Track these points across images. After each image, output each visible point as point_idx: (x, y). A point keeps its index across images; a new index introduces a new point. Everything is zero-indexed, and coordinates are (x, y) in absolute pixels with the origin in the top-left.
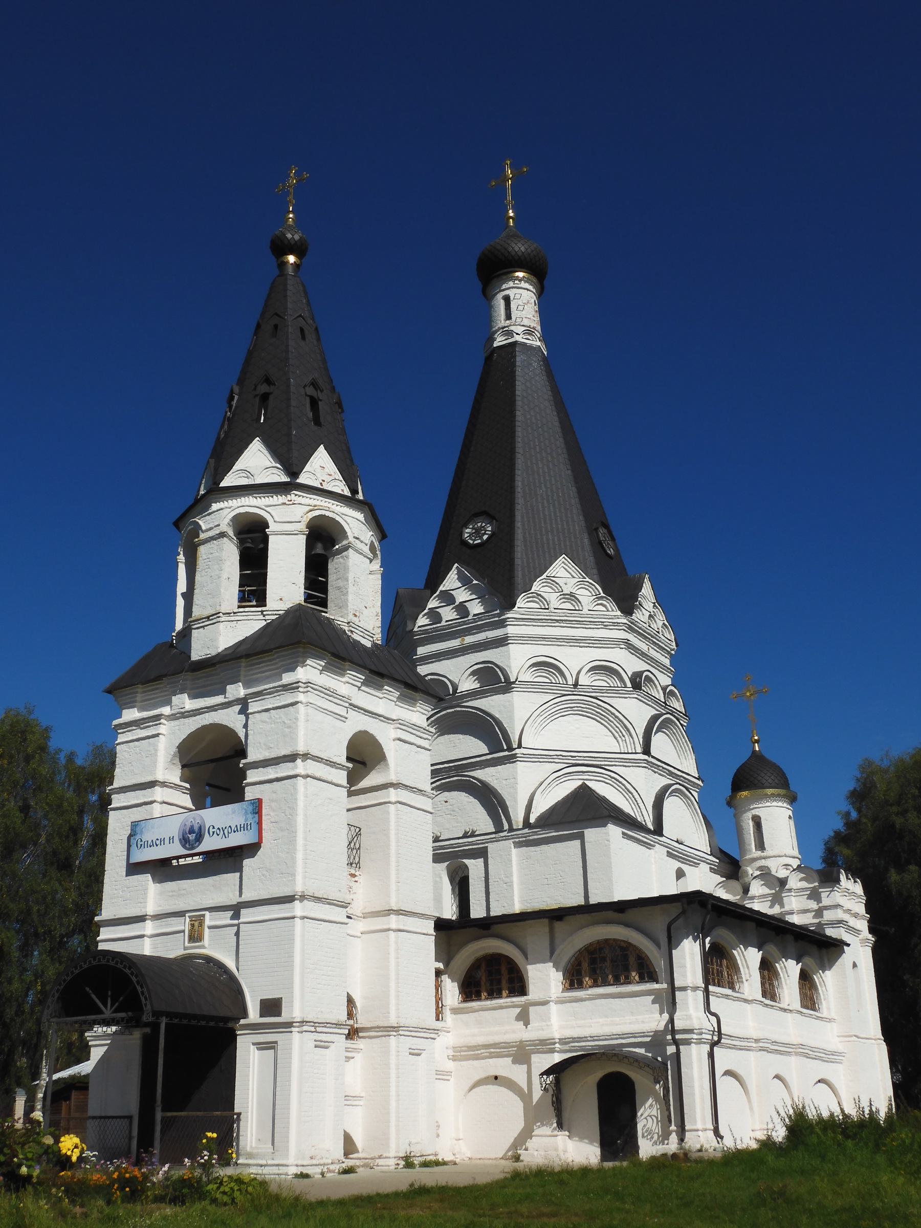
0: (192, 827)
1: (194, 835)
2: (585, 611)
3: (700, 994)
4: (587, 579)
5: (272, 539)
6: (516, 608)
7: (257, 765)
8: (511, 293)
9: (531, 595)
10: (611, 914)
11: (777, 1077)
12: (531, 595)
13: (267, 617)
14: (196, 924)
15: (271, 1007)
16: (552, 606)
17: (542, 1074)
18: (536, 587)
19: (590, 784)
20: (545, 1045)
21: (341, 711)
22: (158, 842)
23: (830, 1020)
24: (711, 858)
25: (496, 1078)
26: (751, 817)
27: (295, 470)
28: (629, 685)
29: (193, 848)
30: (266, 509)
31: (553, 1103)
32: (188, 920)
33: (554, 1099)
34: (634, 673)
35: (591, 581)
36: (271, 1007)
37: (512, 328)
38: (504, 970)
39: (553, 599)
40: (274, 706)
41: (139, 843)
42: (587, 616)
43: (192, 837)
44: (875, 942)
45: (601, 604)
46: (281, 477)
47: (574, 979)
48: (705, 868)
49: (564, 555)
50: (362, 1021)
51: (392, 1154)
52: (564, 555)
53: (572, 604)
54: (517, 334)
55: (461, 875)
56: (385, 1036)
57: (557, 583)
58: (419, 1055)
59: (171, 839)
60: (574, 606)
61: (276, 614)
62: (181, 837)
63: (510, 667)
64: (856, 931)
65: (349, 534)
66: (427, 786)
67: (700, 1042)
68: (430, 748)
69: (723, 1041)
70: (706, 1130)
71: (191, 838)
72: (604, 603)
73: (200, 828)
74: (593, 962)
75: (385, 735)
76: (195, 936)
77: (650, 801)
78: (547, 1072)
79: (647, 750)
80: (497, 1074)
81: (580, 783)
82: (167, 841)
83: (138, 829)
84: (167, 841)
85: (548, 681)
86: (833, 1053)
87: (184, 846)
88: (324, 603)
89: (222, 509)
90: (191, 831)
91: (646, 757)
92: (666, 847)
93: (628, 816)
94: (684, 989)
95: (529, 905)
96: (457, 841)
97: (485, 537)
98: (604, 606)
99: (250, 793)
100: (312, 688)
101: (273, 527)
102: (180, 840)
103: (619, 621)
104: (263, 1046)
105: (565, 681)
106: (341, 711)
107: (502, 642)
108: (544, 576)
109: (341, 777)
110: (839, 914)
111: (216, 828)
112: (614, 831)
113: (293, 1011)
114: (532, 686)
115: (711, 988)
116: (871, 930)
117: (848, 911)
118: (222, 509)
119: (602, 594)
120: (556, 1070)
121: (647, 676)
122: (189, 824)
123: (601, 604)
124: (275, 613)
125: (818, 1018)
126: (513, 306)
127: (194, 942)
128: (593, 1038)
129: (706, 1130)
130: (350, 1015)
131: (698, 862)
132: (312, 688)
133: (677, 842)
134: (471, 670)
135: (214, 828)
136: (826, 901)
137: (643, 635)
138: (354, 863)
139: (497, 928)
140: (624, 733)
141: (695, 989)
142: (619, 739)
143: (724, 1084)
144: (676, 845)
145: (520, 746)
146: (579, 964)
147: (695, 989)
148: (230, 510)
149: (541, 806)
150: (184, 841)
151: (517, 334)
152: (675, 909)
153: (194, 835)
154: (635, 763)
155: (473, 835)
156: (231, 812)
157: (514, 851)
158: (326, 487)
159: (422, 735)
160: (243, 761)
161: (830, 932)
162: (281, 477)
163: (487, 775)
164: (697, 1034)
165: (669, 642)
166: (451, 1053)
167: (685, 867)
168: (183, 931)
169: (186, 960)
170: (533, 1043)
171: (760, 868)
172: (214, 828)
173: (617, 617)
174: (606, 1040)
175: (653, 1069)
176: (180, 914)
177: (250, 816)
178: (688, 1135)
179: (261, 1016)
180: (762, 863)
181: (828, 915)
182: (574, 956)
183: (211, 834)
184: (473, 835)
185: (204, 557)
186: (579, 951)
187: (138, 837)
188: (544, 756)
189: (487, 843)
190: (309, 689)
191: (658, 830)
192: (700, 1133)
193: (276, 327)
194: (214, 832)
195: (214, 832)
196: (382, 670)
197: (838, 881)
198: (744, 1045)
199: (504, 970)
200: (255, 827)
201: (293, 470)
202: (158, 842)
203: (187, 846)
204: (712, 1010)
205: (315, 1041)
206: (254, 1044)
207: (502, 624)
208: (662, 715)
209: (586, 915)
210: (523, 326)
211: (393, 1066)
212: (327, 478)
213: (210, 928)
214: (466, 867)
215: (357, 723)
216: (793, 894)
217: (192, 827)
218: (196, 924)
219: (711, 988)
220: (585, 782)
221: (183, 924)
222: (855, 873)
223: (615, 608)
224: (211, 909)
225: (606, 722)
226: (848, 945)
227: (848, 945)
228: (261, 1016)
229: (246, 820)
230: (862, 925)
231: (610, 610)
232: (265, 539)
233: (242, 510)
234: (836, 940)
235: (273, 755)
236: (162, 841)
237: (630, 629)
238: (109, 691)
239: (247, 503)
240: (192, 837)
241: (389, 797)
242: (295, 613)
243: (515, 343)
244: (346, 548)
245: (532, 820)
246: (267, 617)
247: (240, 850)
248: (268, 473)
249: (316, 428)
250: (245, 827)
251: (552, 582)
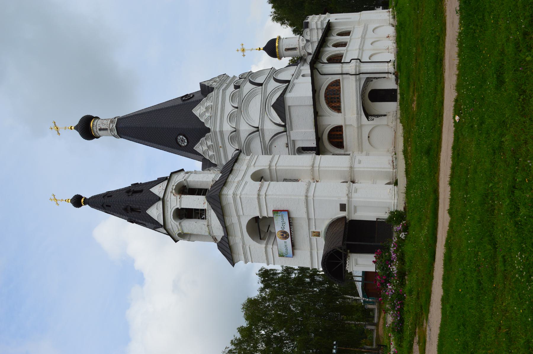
0: (281, 235)
1: (284, 234)
2: (212, 104)
3: (345, 65)
4: (201, 103)
5: (183, 207)
6: (210, 128)
7: (261, 212)
8: (98, 128)
9: (206, 122)
10: (316, 95)
11: (372, 44)
12: (206, 122)
13: (210, 209)
14: (314, 234)
15: (343, 207)
16: (210, 115)
17: (368, 120)
18: (203, 120)
19: (272, 104)
20: (359, 119)
21: (244, 183)
22: (286, 247)
23: (354, 28)
24: (299, 66)
25: (369, 137)
26: (285, 52)
27: (158, 198)
28: (238, 90)
29: (288, 235)
30: (172, 208)
31: (377, 117)
32: (312, 237)
33: (376, 117)
34: (235, 88)
35: (202, 102)
36: (343, 207)
37: (111, 128)
38: (334, 133)
39: (207, 114)
40: (241, 206)
41: (286, 254)
42: (214, 103)
43: (285, 235)
44: (329, 13)
45: (210, 98)
46: (160, 203)
47: (338, 109)
48: (302, 68)
49: (192, 111)
50: (349, 179)
51: (392, 170)
52: (194, 148)
53: (209, 108)
54: (113, 126)
55: (301, 150)
56: (354, 172)
57: (202, 113)
58: (360, 161)
59: (285, 242)
60: (210, 108)
61: (209, 206)
62: (284, 239)
63: (231, 130)
64: (325, 19)
65: (181, 180)
66: (271, 156)
67: (359, 67)
68: (257, 155)
69: (360, 58)
70: (388, 66)
71: (285, 235)
72: (209, 97)
73: (282, 232)
74: (332, 102)
75: (252, 170)
76: (318, 234)
77: (278, 84)
78: (368, 118)
79: (260, 85)
80: (367, 136)
81: (272, 108)
82: (286, 244)
83: (281, 254)
84: (286, 244)
85: (238, 98)
86: (365, 27)
87: (288, 238)
88: (206, 190)
89: (171, 224)
90: (283, 235)
91: (264, 85)
92: (295, 79)
93: (283, 91)
94: (342, 70)
95: (312, 126)
96: (290, 151)
97: (185, 138)
98: (210, 97)
99: (271, 215)
100: (235, 192)
101: (178, 206)
102: (286, 239)
103: (216, 92)
104: (355, 211)
105: (238, 92)
106: (244, 183)
107: (221, 132)
108: (199, 118)
109: (266, 184)
110: (319, 23)
111: (282, 226)
112: (288, 95)
113: (344, 201)
114: (237, 123)
115: (342, 61)
116: (325, 13)
117: (318, 20)
118: (171, 224)
119: (207, 98)
120: (367, 115)
121: (236, 84)
122: (280, 236)
123: (210, 98)
124: (208, 206)
125: (353, 32)
126: (103, 127)
127: (320, 235)
128: (357, 102)
129: (388, 66)
130: (347, 182)
131: (300, 70)
132: (235, 192)
133: (293, 76)
134: (231, 144)
135: (282, 227)
136: (315, 27)
137: (221, 85)
138: (297, 180)
139: (320, 135)
140: (255, 92)
141: (342, 67)
142: (257, 94)
143: (374, 59)
144: (294, 76)
145: (258, 128)
146: (333, 106)
147: (342, 67)
148: (172, 222)
149: (279, 120)
150: (286, 238)
151: (113, 126)
152: (316, 72)
153: (284, 234)
154: (266, 88)
155: (293, 75)
156: (277, 221)
157: (294, 131)
158: (164, 188)
159: (253, 158)
160: (260, 217)
161: (325, 26)
162: (160, 203)
163: (267, 138)
164: (357, 67)
165: (224, 77)
166: (360, 152)
167: (302, 74)
168: (316, 238)
169: (326, 239)
170: (358, 124)
171: (303, 49)
172: (282, 227)
173: (215, 93)
174: (358, 98)
175: (368, 81)
176: (310, 239)
177: (278, 214)
178: (390, 71)
179: (345, 211)
180: (301, 49)
181: (319, 26)
182: (330, 109)
183: (284, 228)
184: (293, 75)
185: (188, 231)
186: (328, 107)
187: (284, 254)
188: (262, 119)
189: (291, 140)
190: (235, 193)
191: (288, 82)
192: (389, 68)
193: (107, 206)
194: (283, 227)
195: (283, 227)
196: (230, 169)
197: (308, 22)
198: (361, 49)
199: (334, 133)
200: (282, 213)
201: (158, 199)
202: (286, 247)
203: (288, 237)
204: (349, 61)
205: (354, 193)
206: (354, 214)
207: (215, 132)
208: (249, 79)
209: (316, 103)
210: (110, 124)
211: (364, 169)
212: (161, 188)
213: (315, 229)
214: (298, 148)
215: (248, 178)
216: (312, 38)
217: (281, 235)
218: (314, 234)
219: (342, 61)
220: (271, 105)
221: (314, 239)
222: (306, 17)
223: (211, 93)
224: (309, 229)
225: (251, 98)
226: (329, 20)
227: (329, 20)
228: (345, 211)
229: (280, 216)
230: (323, 16)
231: (212, 95)
232: (182, 209)
233: (172, 217)
234: (327, 24)
235: (258, 206)
236: (286, 246)
237: (218, 88)
238: (233, 265)
239: (169, 216)
240: (285, 235)
241: (274, 169)
242: (209, 200)
243: (116, 127)
244: (187, 181)
245: (283, 124)
246: (210, 209)
247: (290, 219)
248: (159, 208)
249: (144, 191)
250: (282, 216)
251: (202, 115)
